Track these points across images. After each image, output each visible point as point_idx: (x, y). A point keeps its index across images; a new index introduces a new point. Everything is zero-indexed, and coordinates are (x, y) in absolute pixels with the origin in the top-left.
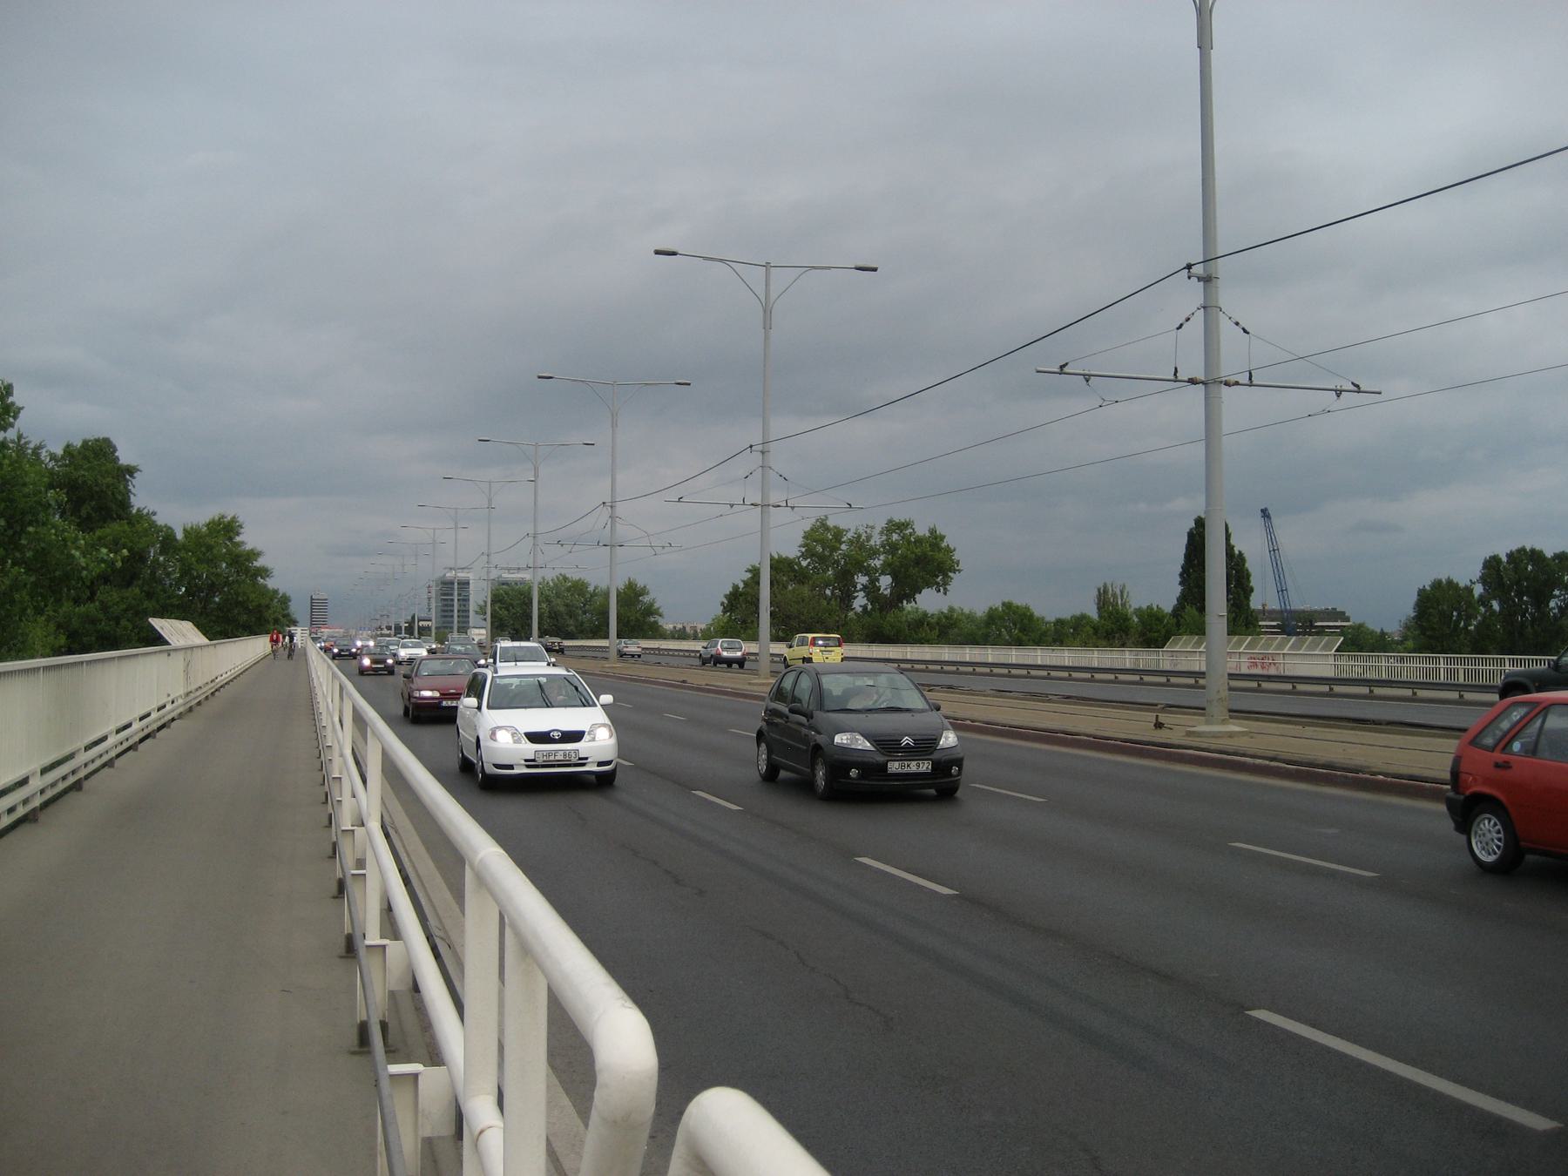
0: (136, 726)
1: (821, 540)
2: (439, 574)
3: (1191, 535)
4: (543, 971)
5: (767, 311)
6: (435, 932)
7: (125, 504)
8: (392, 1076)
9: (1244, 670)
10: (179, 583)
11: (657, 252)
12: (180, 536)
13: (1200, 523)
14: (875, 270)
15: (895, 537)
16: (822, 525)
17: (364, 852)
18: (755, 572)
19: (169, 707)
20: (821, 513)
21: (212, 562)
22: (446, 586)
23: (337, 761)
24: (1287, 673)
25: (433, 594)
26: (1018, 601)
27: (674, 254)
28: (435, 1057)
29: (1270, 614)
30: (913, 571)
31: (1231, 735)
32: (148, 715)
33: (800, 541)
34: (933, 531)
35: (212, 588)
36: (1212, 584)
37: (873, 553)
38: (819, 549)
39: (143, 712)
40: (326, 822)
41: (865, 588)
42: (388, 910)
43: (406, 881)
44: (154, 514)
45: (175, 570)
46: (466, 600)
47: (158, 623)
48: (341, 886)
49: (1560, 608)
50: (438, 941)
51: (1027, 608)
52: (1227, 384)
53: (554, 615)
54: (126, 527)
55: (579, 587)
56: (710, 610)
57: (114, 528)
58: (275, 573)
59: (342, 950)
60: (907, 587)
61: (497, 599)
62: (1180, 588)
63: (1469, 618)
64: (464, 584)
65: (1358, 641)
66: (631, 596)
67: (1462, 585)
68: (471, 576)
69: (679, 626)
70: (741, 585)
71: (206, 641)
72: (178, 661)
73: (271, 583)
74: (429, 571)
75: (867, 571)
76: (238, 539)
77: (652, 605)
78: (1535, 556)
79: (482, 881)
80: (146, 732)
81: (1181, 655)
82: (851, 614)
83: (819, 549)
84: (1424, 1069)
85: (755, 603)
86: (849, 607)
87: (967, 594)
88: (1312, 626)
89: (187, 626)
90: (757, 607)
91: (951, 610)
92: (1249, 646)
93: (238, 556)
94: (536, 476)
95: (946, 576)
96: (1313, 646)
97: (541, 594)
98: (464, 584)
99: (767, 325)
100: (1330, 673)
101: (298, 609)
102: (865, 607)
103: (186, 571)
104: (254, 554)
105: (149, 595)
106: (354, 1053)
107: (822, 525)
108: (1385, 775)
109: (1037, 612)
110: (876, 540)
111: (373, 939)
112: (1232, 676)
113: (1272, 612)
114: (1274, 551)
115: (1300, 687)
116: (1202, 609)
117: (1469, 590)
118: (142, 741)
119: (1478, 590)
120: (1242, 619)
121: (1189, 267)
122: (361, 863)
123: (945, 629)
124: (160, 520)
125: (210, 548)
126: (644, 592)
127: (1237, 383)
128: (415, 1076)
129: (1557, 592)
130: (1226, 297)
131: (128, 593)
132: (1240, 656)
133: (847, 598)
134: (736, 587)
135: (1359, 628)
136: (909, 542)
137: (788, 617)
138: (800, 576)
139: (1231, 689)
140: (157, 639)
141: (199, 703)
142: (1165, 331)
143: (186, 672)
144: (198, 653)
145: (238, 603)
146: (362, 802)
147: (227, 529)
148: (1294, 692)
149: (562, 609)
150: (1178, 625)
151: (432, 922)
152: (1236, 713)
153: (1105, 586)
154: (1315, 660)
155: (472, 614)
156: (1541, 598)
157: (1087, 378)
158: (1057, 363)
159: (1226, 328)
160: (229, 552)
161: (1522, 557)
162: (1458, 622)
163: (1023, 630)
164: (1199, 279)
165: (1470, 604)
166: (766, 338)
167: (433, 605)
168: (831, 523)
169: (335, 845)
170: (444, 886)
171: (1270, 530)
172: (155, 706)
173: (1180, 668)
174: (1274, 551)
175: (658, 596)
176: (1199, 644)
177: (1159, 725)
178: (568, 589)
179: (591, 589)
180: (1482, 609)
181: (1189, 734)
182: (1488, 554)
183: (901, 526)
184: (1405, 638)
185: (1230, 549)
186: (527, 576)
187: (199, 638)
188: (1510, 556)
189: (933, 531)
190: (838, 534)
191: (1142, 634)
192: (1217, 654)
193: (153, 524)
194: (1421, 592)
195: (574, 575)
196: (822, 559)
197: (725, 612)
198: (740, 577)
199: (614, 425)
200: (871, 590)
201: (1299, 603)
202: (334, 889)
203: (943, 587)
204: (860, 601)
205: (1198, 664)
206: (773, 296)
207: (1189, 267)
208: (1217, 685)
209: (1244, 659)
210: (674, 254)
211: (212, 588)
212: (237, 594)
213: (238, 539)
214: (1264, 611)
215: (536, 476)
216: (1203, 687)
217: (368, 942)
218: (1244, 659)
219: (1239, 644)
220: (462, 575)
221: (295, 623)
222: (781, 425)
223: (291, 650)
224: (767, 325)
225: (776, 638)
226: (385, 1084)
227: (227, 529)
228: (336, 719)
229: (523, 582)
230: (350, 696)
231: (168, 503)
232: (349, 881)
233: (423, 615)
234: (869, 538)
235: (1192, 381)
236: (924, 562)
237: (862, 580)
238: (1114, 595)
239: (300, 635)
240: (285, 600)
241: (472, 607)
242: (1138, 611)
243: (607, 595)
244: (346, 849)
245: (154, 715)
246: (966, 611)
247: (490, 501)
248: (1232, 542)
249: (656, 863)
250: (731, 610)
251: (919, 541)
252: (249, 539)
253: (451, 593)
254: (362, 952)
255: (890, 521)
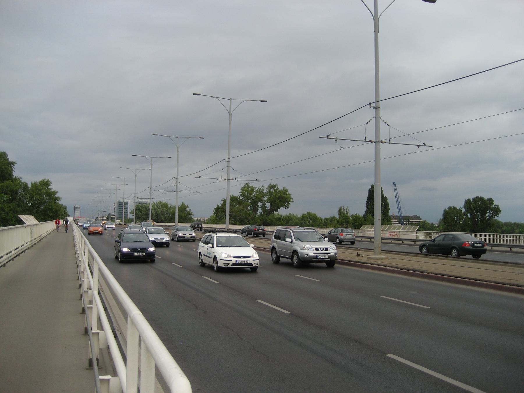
0: (13, 252)
1: (247, 190)
2: (118, 200)
3: (369, 191)
4: (154, 359)
5: (230, 115)
6: (116, 328)
7: (11, 175)
8: (93, 333)
9: (387, 237)
10: (29, 202)
11: (194, 94)
12: (30, 186)
13: (373, 187)
14: (266, 101)
15: (272, 190)
16: (248, 185)
17: (92, 298)
18: (225, 201)
19: (25, 245)
20: (247, 182)
21: (41, 195)
22: (120, 203)
23: (82, 266)
24: (401, 238)
25: (116, 207)
26: (312, 212)
27: (199, 95)
28: (115, 373)
29: (395, 217)
30: (277, 201)
31: (382, 259)
32: (18, 248)
33: (240, 191)
34: (284, 188)
35: (40, 204)
36: (377, 207)
37: (264, 195)
38: (246, 194)
39: (16, 247)
40: (78, 287)
41: (261, 207)
42: (99, 320)
43: (105, 309)
44: (21, 178)
45: (27, 196)
46: (127, 209)
47: (22, 217)
48: (84, 310)
49: (489, 216)
50: (117, 332)
51: (315, 214)
52: (382, 143)
53: (157, 214)
54: (11, 183)
55: (165, 205)
56: (209, 213)
57: (7, 183)
58: (62, 198)
59: (83, 332)
60: (275, 207)
61: (138, 209)
62: (366, 208)
63: (460, 219)
64: (127, 203)
65: (424, 227)
66: (183, 208)
67: (458, 208)
68: (129, 201)
69: (199, 219)
70: (220, 205)
71: (38, 222)
72: (28, 230)
73: (60, 202)
74: (114, 199)
75: (262, 201)
76: (50, 187)
77: (190, 211)
78: (481, 199)
79: (133, 323)
80: (17, 254)
81: (366, 231)
82: (257, 215)
83: (246, 194)
84: (444, 374)
85: (224, 211)
86: (256, 213)
87: (295, 209)
88: (409, 221)
89: (32, 217)
90: (225, 213)
91: (290, 214)
92: (389, 228)
93: (49, 193)
94: (152, 167)
95: (288, 203)
96: (409, 229)
97: (153, 207)
98: (127, 203)
99: (230, 119)
100: (415, 238)
101: (70, 211)
102: (261, 213)
103: (32, 198)
104: (55, 192)
105: (19, 206)
106: (87, 369)
107: (248, 185)
108: (432, 273)
109: (319, 215)
110: (265, 191)
111: (95, 330)
112: (383, 238)
113: (396, 216)
114: (397, 196)
115: (405, 242)
116: (373, 215)
117: (460, 210)
118: (15, 257)
119: (463, 210)
120: (386, 219)
121: (370, 104)
122: (90, 302)
123: (288, 221)
124: (23, 180)
125: (40, 190)
126: (187, 207)
127: (385, 142)
128: (108, 380)
129: (488, 211)
130: (382, 113)
131: (11, 205)
132: (386, 232)
133: (255, 210)
134: (218, 206)
135: (424, 222)
136: (276, 192)
137: (236, 216)
138: (240, 203)
139: (382, 243)
140: (20, 222)
141: (35, 244)
142: (361, 124)
143: (31, 233)
144: (35, 227)
145: (49, 209)
146: (91, 283)
147: (46, 184)
148: (403, 244)
149: (159, 212)
150: (365, 220)
151: (115, 325)
152: (384, 251)
153: (341, 207)
154: (410, 233)
155: (129, 213)
156: (483, 214)
157: (336, 140)
158: (325, 134)
159: (382, 125)
160: (47, 192)
161: (478, 199)
162: (457, 220)
163: (314, 221)
164: (373, 108)
165: (461, 215)
166: (230, 123)
167: (116, 210)
168: (250, 185)
169: (81, 295)
170: (118, 309)
171: (395, 189)
172: (20, 245)
173: (366, 235)
174: (397, 196)
175: (192, 208)
176: (372, 228)
177: (358, 255)
178: (162, 206)
179: (169, 206)
180: (465, 217)
181: (368, 258)
182: (466, 198)
183: (274, 186)
184: (439, 225)
185: (382, 195)
186: (148, 201)
187: (36, 222)
188: (474, 199)
189: (284, 188)
190: (253, 188)
191: (353, 223)
192: (376, 231)
193: (20, 182)
194: (445, 211)
195: (164, 201)
196: (247, 197)
197: (214, 214)
198: (220, 203)
199: (178, 151)
200: (263, 207)
201: (404, 214)
202: (81, 311)
203: (287, 207)
204: (260, 211)
205: (371, 234)
206: (233, 108)
207: (370, 104)
208: (377, 242)
209: (387, 233)
210: (199, 95)
211: (40, 204)
212: (49, 206)
213: (50, 187)
214: (393, 216)
215: (152, 167)
216: (373, 242)
217: (93, 331)
218: (387, 233)
219: (385, 228)
220: (126, 200)
221: (68, 216)
222: (234, 152)
223: (67, 227)
224: (230, 119)
225: (231, 223)
226: (98, 383)
227: (46, 184)
228: (83, 252)
229: (146, 203)
230: (88, 246)
231: (26, 174)
232: (86, 309)
233: (113, 213)
234: (263, 190)
235: (371, 142)
236: (281, 198)
237: (260, 204)
238: (344, 210)
239: (70, 219)
240: (65, 208)
241: (129, 211)
242: (352, 216)
243: (175, 208)
244: (85, 297)
245: (20, 248)
246: (295, 215)
247: (136, 176)
248: (383, 193)
249: (190, 302)
250: (217, 214)
251: (280, 191)
252: (53, 187)
253: (122, 206)
254: (91, 335)
255: (270, 185)
